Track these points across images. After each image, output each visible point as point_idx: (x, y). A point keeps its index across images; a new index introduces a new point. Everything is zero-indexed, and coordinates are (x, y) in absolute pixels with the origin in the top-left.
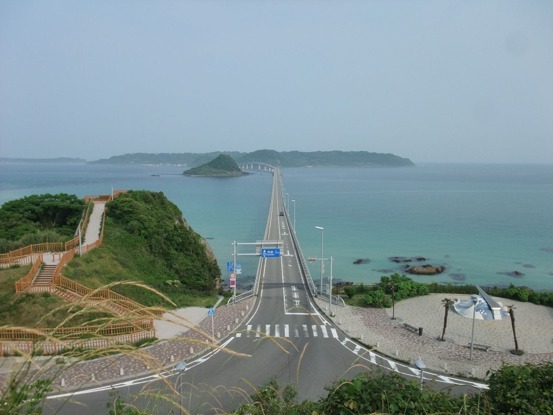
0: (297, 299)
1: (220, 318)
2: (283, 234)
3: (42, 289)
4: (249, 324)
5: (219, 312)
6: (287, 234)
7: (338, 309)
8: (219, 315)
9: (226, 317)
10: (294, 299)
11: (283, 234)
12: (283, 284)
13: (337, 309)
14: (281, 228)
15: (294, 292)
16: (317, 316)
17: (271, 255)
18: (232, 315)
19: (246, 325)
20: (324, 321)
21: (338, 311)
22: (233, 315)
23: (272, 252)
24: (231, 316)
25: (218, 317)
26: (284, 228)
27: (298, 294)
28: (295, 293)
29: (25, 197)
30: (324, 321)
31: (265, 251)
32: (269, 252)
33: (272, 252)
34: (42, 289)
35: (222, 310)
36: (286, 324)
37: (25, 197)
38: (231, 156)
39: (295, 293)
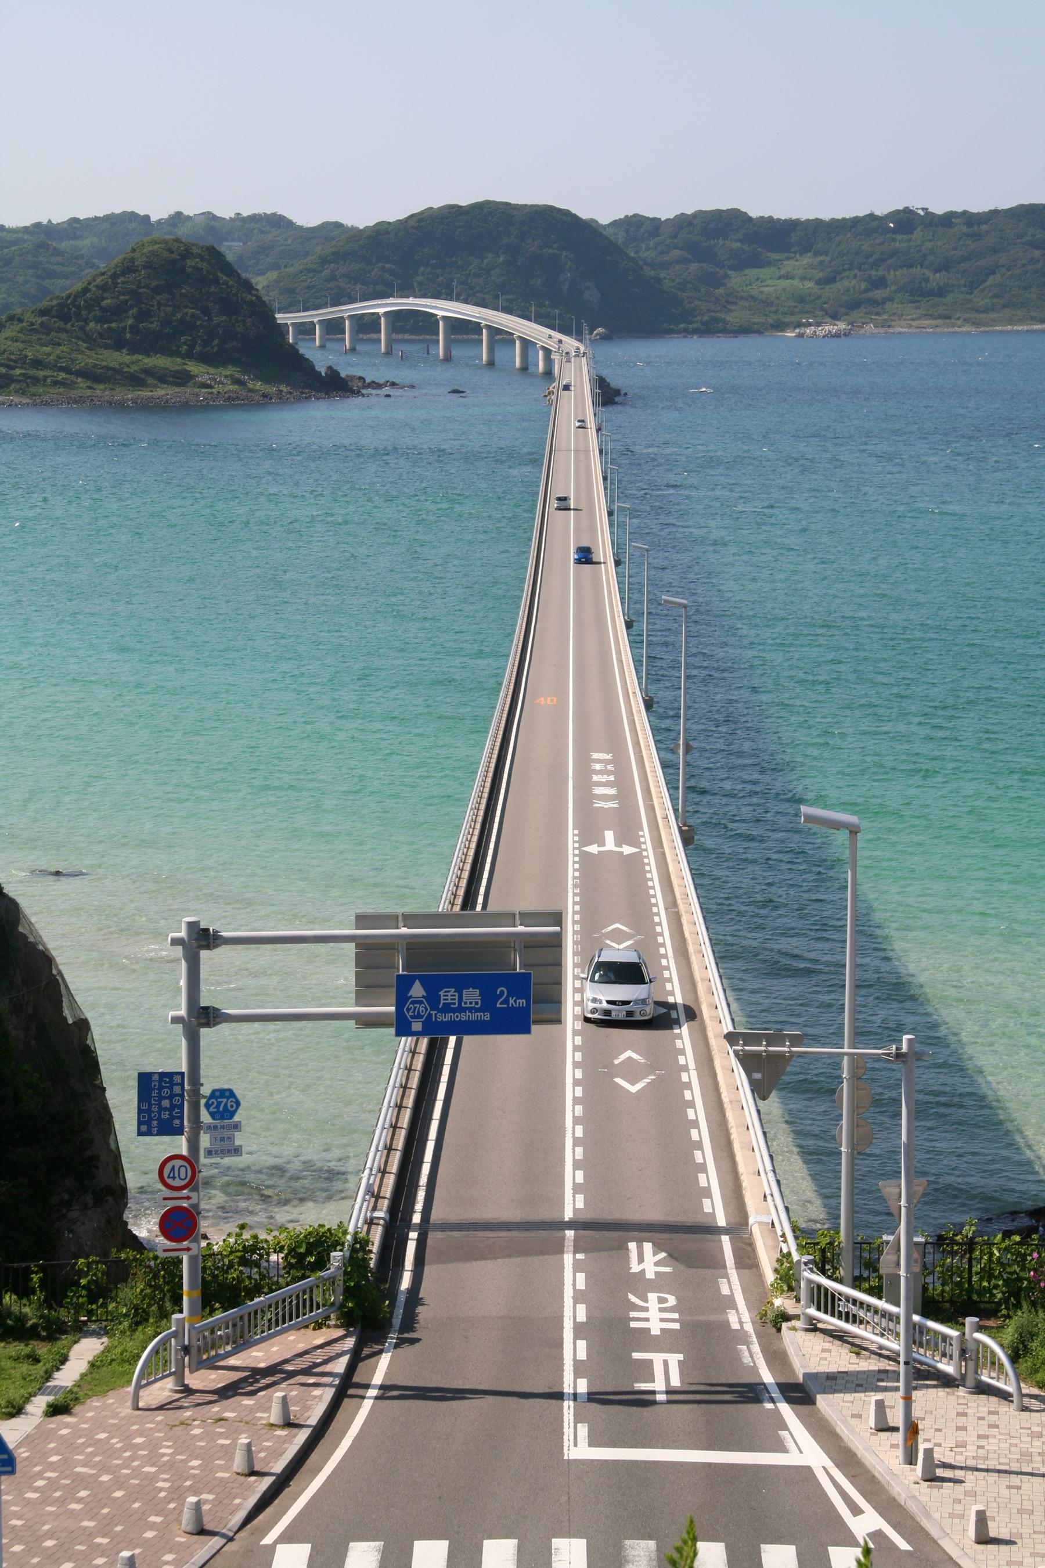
0: (666, 1342)
1: (70, 1495)
2: (593, 849)
3: (604, 778)
4: (287, 1537)
5: (68, 1446)
6: (627, 850)
7: (970, 1422)
8: (66, 1464)
9: (119, 1483)
10: (643, 1339)
11: (593, 849)
12: (572, 1225)
13: (961, 1421)
14: (585, 799)
15: (640, 1284)
16: (805, 1474)
17: (464, 1017)
18: (163, 1468)
19: (268, 1540)
20: (856, 1511)
21: (971, 1437)
22: (171, 1466)
23: (472, 996)
24: (152, 1478)
25: (52, 1484)
26: (605, 798)
27: (672, 1300)
28: (652, 1297)
29: (50, 221)
30: (856, 1511)
31: (417, 990)
32: (448, 995)
33: (472, 996)
34: (604, 778)
35: (90, 1434)
36: (569, 1535)
37: (50, 221)
38: (231, 250)
39: (652, 1297)
